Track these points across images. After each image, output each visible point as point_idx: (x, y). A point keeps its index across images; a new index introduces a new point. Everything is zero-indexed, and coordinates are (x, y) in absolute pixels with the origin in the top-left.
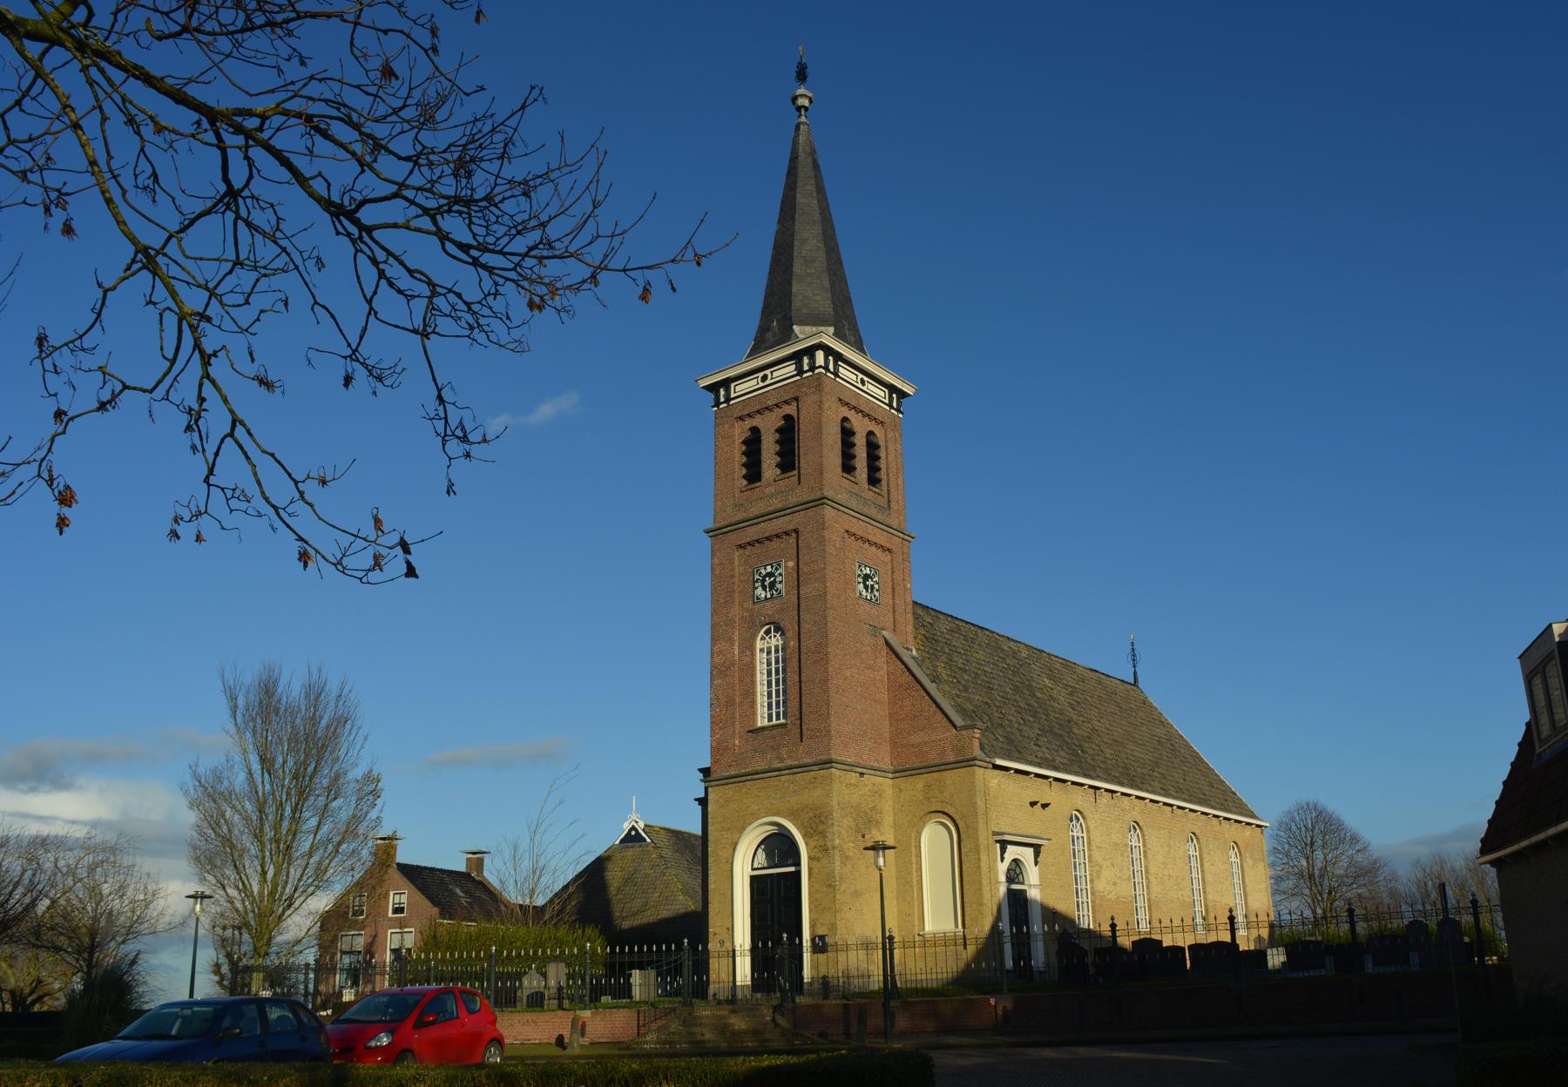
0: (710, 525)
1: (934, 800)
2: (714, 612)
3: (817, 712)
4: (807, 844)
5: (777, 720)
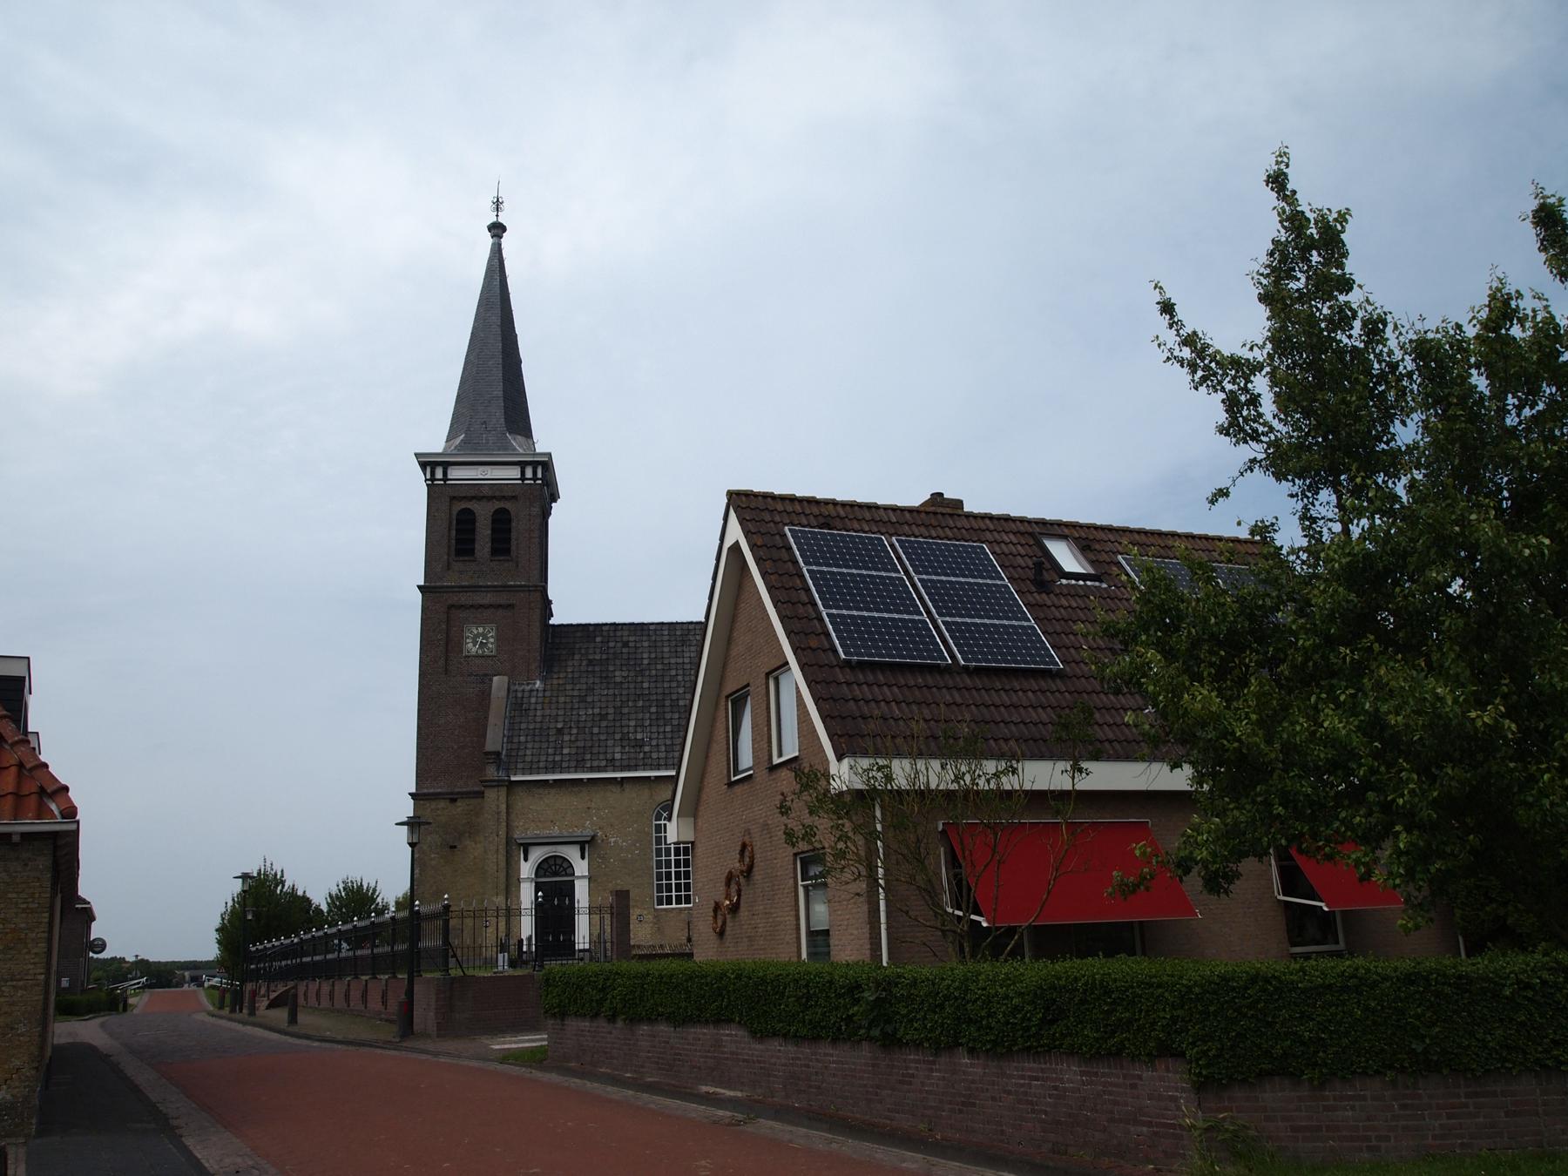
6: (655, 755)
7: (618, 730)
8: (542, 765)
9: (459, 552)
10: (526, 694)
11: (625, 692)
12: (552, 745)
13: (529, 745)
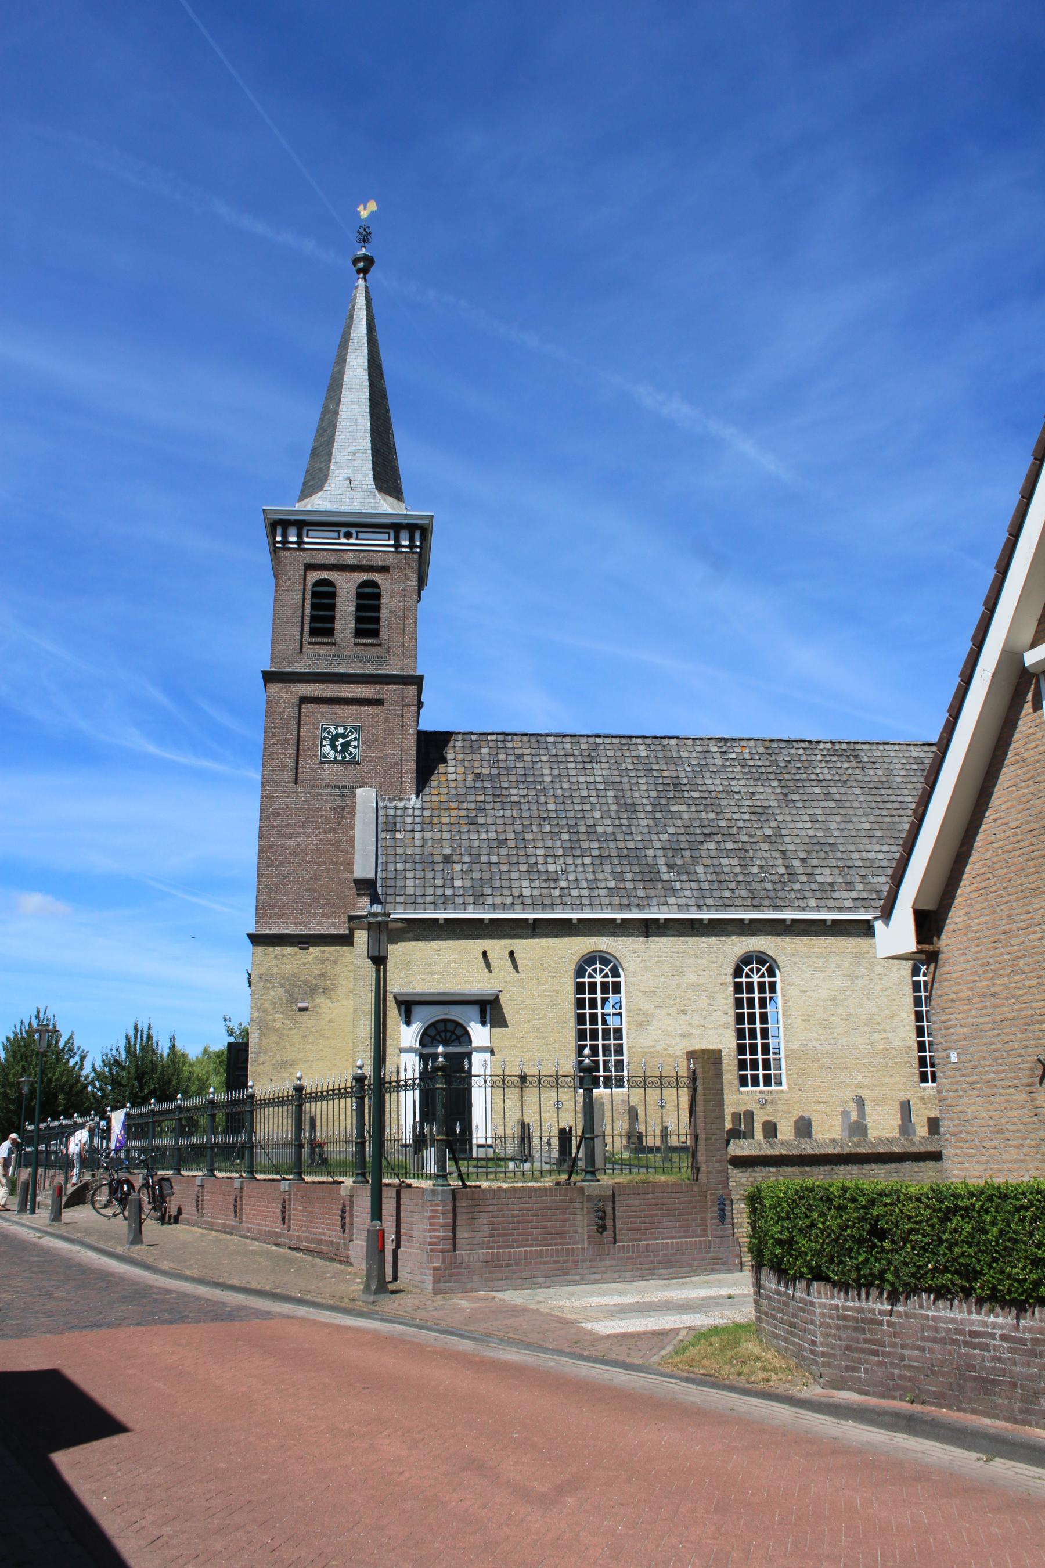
6: (575, 893)
7: (523, 860)
8: (429, 899)
9: (314, 632)
10: (399, 812)
11: (526, 814)
12: (439, 875)
13: (410, 875)
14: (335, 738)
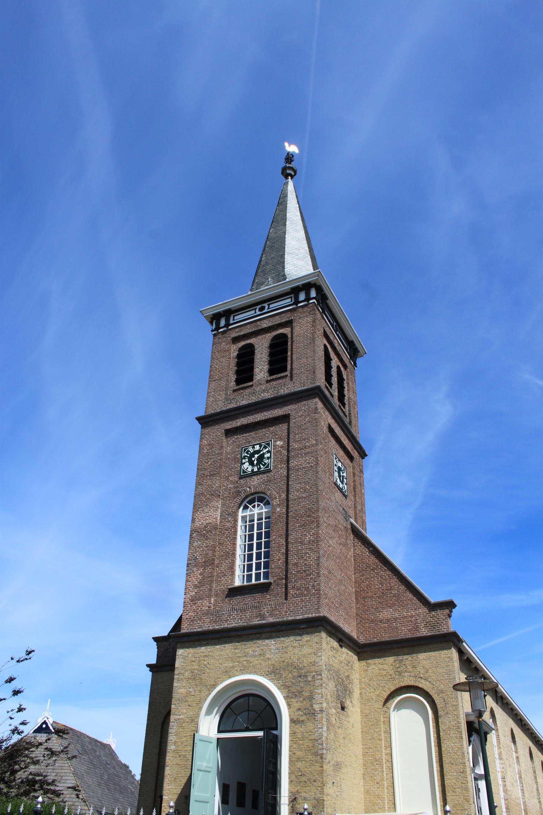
0: (202, 413)
1: (406, 674)
2: (198, 484)
3: (305, 571)
4: (289, 705)
5: (256, 580)
14: (252, 455)
